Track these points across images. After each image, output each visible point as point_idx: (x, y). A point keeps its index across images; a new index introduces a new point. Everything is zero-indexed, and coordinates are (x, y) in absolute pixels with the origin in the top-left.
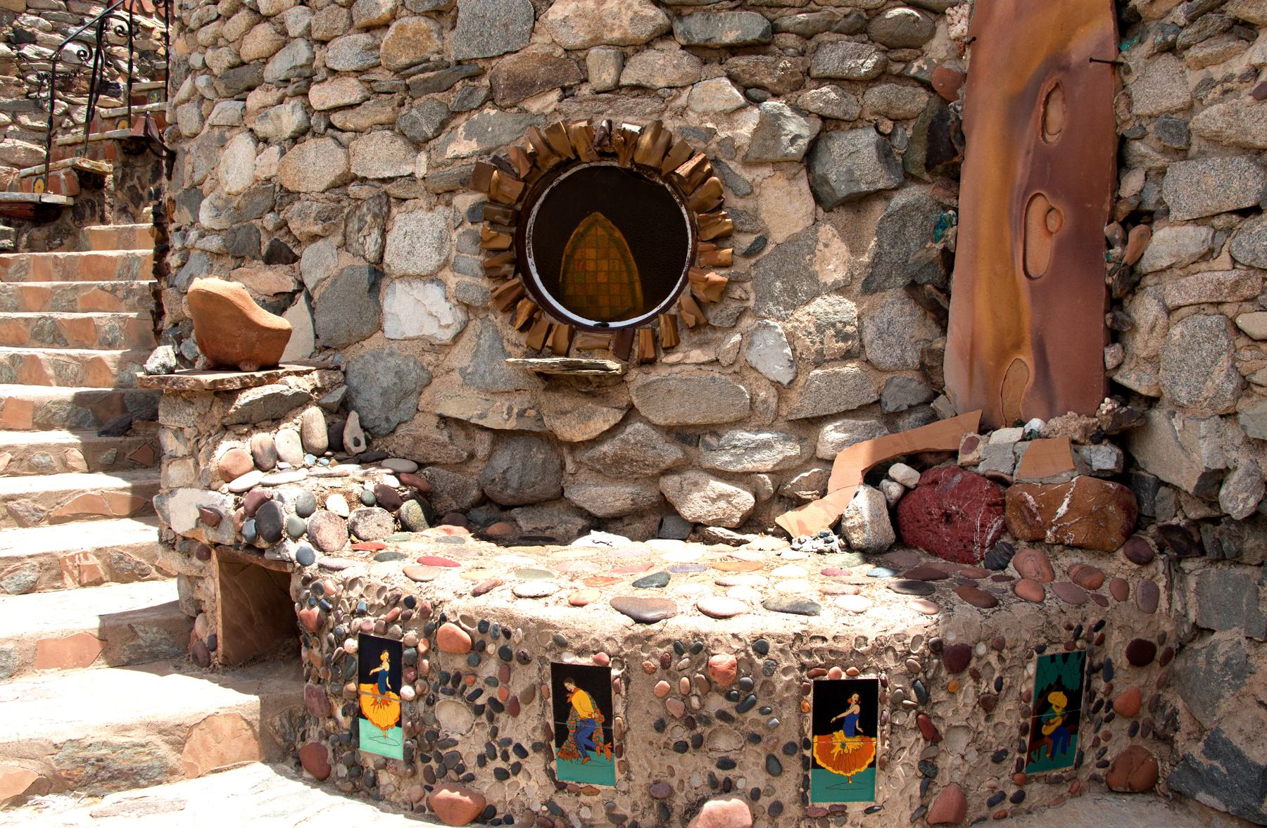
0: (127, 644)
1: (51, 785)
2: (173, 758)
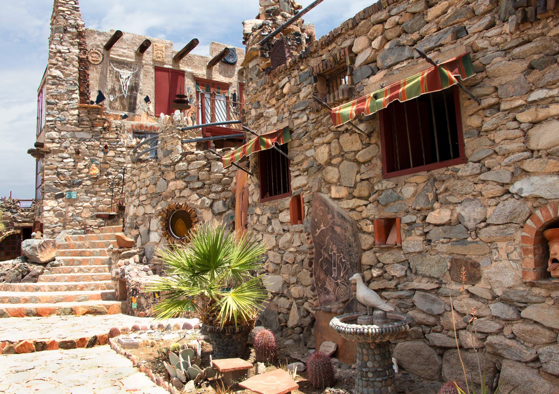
0: (105, 297)
1: (88, 312)
2: (107, 311)
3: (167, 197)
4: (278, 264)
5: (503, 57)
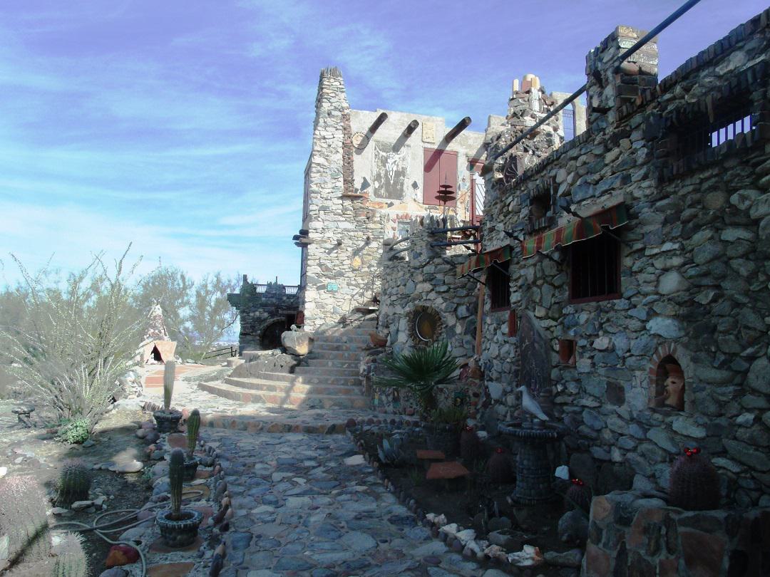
3: (414, 299)
4: (500, 373)
5: (649, 208)
